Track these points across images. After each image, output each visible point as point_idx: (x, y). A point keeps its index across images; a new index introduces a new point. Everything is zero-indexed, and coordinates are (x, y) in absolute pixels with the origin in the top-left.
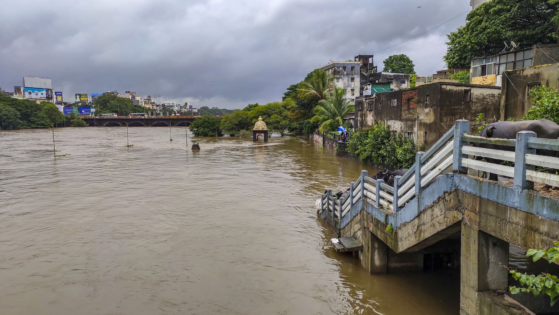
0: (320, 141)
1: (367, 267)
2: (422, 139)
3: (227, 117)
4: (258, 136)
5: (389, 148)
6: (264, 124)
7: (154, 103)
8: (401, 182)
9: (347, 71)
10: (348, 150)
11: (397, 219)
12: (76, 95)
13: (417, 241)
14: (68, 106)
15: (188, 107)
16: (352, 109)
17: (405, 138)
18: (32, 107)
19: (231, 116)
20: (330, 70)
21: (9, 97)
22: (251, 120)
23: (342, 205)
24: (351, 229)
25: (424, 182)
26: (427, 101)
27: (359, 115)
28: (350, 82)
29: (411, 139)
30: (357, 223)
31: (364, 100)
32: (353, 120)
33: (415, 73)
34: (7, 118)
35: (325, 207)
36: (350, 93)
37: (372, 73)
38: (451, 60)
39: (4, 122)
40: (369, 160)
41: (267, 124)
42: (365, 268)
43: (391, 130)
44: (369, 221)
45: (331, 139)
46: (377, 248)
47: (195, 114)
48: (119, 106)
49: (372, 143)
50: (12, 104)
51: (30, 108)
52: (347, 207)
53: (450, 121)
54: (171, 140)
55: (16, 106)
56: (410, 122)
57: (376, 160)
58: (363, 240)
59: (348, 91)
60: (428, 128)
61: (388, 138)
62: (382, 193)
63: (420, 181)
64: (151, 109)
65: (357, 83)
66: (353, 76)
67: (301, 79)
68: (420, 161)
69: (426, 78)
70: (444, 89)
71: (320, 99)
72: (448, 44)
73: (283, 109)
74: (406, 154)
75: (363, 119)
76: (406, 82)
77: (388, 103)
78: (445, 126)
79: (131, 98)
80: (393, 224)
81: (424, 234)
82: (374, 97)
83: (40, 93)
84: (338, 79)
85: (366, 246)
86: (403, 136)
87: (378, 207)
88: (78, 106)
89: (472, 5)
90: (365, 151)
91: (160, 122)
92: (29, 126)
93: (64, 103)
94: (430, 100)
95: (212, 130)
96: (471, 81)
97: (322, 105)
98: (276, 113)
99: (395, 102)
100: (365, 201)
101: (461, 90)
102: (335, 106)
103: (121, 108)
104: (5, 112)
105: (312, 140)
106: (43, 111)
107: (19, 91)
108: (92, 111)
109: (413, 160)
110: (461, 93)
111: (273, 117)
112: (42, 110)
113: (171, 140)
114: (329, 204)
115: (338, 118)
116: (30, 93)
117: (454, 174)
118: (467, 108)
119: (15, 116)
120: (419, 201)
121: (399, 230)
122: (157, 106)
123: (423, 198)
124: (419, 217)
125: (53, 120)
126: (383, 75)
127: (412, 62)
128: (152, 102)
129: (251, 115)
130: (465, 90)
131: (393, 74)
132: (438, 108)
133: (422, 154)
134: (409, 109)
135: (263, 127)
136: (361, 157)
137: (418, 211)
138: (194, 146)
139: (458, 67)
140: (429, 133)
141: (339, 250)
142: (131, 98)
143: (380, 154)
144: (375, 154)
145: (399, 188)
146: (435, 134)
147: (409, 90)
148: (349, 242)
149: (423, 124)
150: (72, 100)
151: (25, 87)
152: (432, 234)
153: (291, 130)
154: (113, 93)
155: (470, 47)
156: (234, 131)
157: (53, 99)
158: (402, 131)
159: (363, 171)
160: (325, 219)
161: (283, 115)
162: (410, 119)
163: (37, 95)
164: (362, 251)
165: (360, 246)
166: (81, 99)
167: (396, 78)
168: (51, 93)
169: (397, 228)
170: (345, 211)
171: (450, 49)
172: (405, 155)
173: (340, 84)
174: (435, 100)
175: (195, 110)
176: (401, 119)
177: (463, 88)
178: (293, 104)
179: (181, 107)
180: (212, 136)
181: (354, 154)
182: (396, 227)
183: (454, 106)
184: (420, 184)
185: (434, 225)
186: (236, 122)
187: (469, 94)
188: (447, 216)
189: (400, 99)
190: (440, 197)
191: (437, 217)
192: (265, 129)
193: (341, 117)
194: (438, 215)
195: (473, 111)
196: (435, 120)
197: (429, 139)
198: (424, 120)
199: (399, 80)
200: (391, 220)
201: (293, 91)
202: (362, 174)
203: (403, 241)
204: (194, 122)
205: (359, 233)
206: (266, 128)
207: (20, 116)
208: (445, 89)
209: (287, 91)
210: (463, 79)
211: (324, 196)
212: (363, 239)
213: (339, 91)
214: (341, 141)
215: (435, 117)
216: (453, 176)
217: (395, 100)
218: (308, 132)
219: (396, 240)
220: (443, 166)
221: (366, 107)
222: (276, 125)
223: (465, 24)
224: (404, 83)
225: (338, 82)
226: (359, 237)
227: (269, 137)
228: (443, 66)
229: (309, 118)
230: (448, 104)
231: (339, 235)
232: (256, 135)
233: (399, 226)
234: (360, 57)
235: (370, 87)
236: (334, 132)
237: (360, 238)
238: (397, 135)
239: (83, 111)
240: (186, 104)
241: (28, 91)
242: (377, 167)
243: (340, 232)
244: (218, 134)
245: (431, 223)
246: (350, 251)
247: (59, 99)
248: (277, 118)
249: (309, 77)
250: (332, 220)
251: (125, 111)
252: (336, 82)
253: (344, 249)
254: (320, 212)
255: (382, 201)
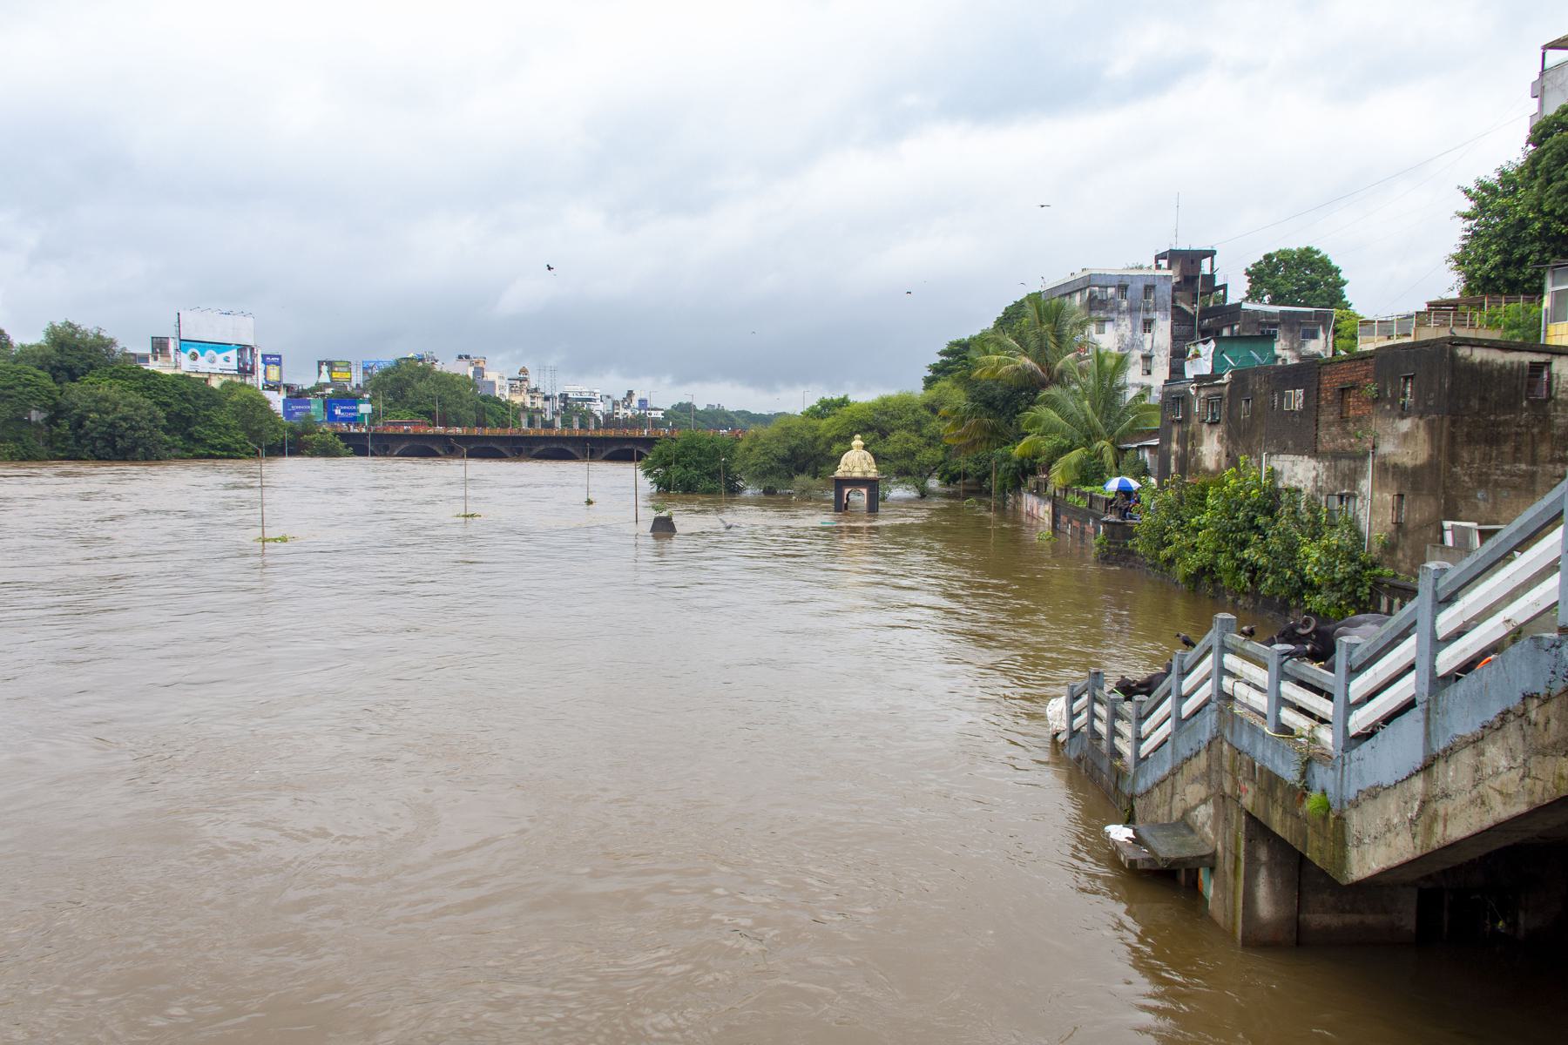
0: (1042, 516)
1: (1229, 922)
2: (1389, 519)
3: (757, 436)
4: (848, 495)
5: (1276, 544)
6: (870, 458)
7: (536, 390)
8: (1362, 655)
9: (1131, 298)
10: (1137, 545)
11: (1346, 773)
12: (320, 363)
13: (1418, 848)
14: (296, 396)
15: (635, 404)
16: (1149, 418)
17: (1330, 513)
18: (198, 397)
19: (766, 432)
20: (1078, 297)
21: (138, 368)
22: (829, 445)
23: (1142, 719)
24: (1172, 797)
25: (1448, 659)
26: (1404, 395)
27: (1175, 436)
28: (1139, 333)
29: (1350, 516)
30: (1194, 780)
31: (1191, 390)
32: (1151, 453)
33: (1347, 306)
34: (131, 428)
35: (1077, 722)
36: (1137, 366)
37: (1211, 305)
38: (1477, 266)
39: (122, 437)
40: (1206, 577)
41: (877, 458)
42: (1222, 925)
43: (1280, 485)
44: (1240, 778)
45: (1076, 511)
46: (1265, 864)
47: (656, 423)
48: (439, 397)
49: (1219, 526)
50: (144, 387)
51: (192, 398)
52: (1158, 728)
53: (1483, 460)
54: (589, 502)
55: (155, 393)
56: (1346, 464)
57: (1232, 579)
58: (1216, 834)
59: (1132, 360)
60: (1407, 481)
61: (1270, 512)
62: (1289, 690)
63: (1434, 656)
64: (528, 409)
65: (1162, 334)
66: (1151, 314)
67: (985, 321)
68: (1435, 594)
69: (1435, 323)
70: (1462, 361)
71: (1044, 385)
72: (1467, 217)
73: (926, 413)
74: (1335, 561)
75: (1189, 448)
76: (1322, 336)
77: (1273, 401)
78: (1465, 475)
79: (471, 375)
80: (1331, 789)
81: (1445, 826)
82: (1225, 381)
83: (220, 357)
84: (1102, 322)
85: (1228, 854)
86: (1324, 504)
87: (1276, 732)
88: (323, 396)
89: (1536, 97)
90: (1194, 548)
91: (555, 446)
92: (187, 451)
93: (284, 385)
94: (1417, 393)
95: (708, 474)
96: (1546, 336)
97: (1052, 403)
98: (904, 427)
99: (1296, 399)
100: (1228, 713)
101: (1520, 364)
102: (1093, 406)
103: (443, 405)
104: (126, 408)
105: (1016, 510)
106: (227, 409)
107: (163, 351)
108: (361, 411)
109: (1355, 583)
110: (1521, 371)
111: (895, 438)
112: (226, 407)
113: (589, 502)
114: (1093, 715)
115: (1098, 445)
116: (194, 357)
117: (1563, 638)
118: (1540, 421)
119: (150, 421)
120: (1428, 720)
121: (1352, 810)
122: (547, 399)
123: (1446, 712)
124: (1427, 771)
125: (255, 435)
126: (1247, 312)
127: (1337, 271)
128: (533, 386)
129: (829, 431)
130: (1531, 363)
131: (1276, 309)
132: (1443, 417)
133: (1443, 571)
134: (1343, 419)
135: (866, 467)
136: (1180, 570)
137: (1424, 752)
138: (657, 520)
139: (1497, 291)
140: (1410, 497)
141: (1133, 863)
142: (471, 375)
143: (1244, 561)
144: (1227, 559)
145: (1354, 675)
146: (1432, 500)
147: (1343, 361)
148: (1169, 840)
149: (1391, 469)
150: (306, 381)
151: (181, 340)
152: (1475, 828)
153: (951, 478)
154: (422, 360)
155: (1537, 225)
156: (775, 478)
157: (191, 374)
158: (1319, 490)
159: (1220, 616)
160: (1079, 760)
161: (925, 431)
162: (1347, 452)
163: (213, 362)
164: (1212, 869)
165: (1206, 853)
166: (334, 375)
167: (1289, 321)
168: (251, 355)
169: (1346, 803)
170: (1150, 740)
171: (1470, 233)
172: (1332, 566)
173: (1108, 339)
174: (1432, 395)
175: (655, 412)
176: (1316, 451)
177: (1527, 358)
178: (958, 397)
179: (615, 404)
180: (709, 492)
181: (1157, 558)
182: (1342, 802)
183: (1495, 414)
184: (1433, 667)
185: (1482, 801)
186: (782, 451)
187: (1545, 376)
188: (1533, 773)
189: (1316, 387)
190: (1508, 711)
191: (1496, 774)
192: (870, 475)
193: (1113, 443)
194: (1501, 769)
195: (1558, 430)
196: (1431, 456)
197: (1412, 516)
198: (1395, 457)
199: (1297, 328)
200: (1323, 777)
201: (958, 357)
202: (1216, 627)
203: (1367, 846)
204: (657, 448)
205: (1203, 814)
206: (873, 473)
207: (164, 422)
208: (1466, 359)
209: (937, 359)
210: (1517, 328)
211: (1076, 689)
212: (1216, 833)
213: (1110, 363)
214: (1112, 518)
215: (1433, 449)
216: (1557, 644)
217: (1300, 392)
218: (1005, 486)
219: (1341, 843)
220: (1520, 610)
221: (1197, 411)
222: (904, 462)
223: (1521, 156)
224: (1314, 336)
225: (1101, 331)
226: (1203, 824)
227: (884, 499)
228: (1449, 285)
229: (1007, 444)
230: (1477, 407)
231: (1130, 816)
232: (843, 492)
233: (1352, 797)
234: (1173, 256)
235: (1208, 350)
236: (1088, 489)
237: (1207, 829)
238: (1302, 504)
239: (338, 412)
240: (630, 394)
241: (190, 351)
242: (1234, 602)
243: (1132, 807)
244: (726, 487)
245: (1474, 793)
246: (1174, 868)
247: (274, 374)
248: (907, 440)
249: (1011, 318)
250: (1105, 765)
251: (456, 414)
252: (1094, 332)
253: (1149, 860)
254: (1061, 738)
255: (1288, 716)
